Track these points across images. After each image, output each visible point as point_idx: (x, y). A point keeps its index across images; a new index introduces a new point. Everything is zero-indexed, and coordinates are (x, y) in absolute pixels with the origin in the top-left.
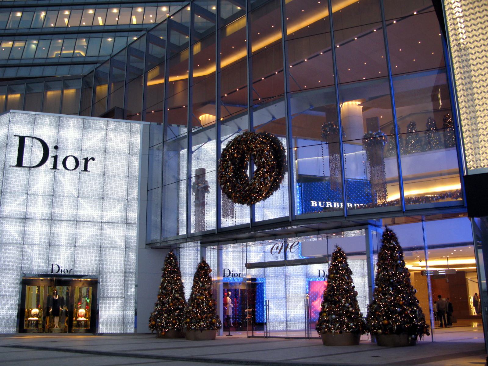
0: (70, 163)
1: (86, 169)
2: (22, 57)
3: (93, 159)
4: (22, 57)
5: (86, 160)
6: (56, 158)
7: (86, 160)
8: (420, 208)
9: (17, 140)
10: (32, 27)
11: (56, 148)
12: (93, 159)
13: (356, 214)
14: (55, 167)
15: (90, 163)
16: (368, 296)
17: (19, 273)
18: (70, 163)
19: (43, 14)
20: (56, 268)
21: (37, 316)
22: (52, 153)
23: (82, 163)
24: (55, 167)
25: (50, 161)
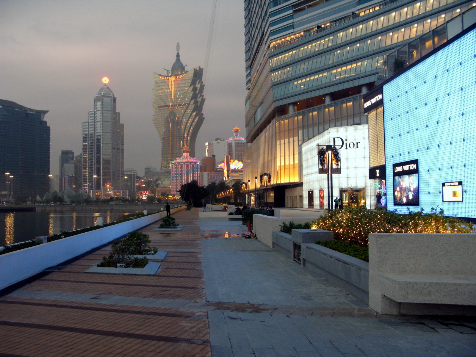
0: (352, 145)
1: (357, 147)
2: (313, 129)
3: (359, 142)
4: (313, 129)
5: (357, 143)
6: (346, 144)
7: (357, 143)
8: (150, 223)
9: (333, 139)
10: (364, 52)
11: (346, 140)
12: (359, 142)
13: (144, 225)
14: (346, 148)
15: (359, 144)
16: (17, 206)
17: (338, 188)
18: (352, 145)
19: (369, 42)
20: (350, 186)
21: (347, 203)
22: (345, 142)
23: (356, 145)
24: (346, 148)
25: (344, 145)
